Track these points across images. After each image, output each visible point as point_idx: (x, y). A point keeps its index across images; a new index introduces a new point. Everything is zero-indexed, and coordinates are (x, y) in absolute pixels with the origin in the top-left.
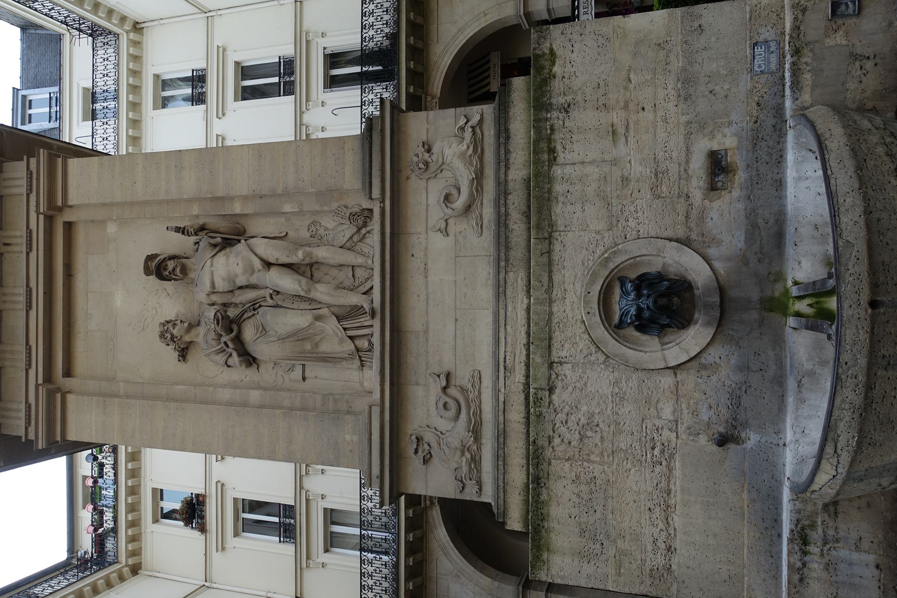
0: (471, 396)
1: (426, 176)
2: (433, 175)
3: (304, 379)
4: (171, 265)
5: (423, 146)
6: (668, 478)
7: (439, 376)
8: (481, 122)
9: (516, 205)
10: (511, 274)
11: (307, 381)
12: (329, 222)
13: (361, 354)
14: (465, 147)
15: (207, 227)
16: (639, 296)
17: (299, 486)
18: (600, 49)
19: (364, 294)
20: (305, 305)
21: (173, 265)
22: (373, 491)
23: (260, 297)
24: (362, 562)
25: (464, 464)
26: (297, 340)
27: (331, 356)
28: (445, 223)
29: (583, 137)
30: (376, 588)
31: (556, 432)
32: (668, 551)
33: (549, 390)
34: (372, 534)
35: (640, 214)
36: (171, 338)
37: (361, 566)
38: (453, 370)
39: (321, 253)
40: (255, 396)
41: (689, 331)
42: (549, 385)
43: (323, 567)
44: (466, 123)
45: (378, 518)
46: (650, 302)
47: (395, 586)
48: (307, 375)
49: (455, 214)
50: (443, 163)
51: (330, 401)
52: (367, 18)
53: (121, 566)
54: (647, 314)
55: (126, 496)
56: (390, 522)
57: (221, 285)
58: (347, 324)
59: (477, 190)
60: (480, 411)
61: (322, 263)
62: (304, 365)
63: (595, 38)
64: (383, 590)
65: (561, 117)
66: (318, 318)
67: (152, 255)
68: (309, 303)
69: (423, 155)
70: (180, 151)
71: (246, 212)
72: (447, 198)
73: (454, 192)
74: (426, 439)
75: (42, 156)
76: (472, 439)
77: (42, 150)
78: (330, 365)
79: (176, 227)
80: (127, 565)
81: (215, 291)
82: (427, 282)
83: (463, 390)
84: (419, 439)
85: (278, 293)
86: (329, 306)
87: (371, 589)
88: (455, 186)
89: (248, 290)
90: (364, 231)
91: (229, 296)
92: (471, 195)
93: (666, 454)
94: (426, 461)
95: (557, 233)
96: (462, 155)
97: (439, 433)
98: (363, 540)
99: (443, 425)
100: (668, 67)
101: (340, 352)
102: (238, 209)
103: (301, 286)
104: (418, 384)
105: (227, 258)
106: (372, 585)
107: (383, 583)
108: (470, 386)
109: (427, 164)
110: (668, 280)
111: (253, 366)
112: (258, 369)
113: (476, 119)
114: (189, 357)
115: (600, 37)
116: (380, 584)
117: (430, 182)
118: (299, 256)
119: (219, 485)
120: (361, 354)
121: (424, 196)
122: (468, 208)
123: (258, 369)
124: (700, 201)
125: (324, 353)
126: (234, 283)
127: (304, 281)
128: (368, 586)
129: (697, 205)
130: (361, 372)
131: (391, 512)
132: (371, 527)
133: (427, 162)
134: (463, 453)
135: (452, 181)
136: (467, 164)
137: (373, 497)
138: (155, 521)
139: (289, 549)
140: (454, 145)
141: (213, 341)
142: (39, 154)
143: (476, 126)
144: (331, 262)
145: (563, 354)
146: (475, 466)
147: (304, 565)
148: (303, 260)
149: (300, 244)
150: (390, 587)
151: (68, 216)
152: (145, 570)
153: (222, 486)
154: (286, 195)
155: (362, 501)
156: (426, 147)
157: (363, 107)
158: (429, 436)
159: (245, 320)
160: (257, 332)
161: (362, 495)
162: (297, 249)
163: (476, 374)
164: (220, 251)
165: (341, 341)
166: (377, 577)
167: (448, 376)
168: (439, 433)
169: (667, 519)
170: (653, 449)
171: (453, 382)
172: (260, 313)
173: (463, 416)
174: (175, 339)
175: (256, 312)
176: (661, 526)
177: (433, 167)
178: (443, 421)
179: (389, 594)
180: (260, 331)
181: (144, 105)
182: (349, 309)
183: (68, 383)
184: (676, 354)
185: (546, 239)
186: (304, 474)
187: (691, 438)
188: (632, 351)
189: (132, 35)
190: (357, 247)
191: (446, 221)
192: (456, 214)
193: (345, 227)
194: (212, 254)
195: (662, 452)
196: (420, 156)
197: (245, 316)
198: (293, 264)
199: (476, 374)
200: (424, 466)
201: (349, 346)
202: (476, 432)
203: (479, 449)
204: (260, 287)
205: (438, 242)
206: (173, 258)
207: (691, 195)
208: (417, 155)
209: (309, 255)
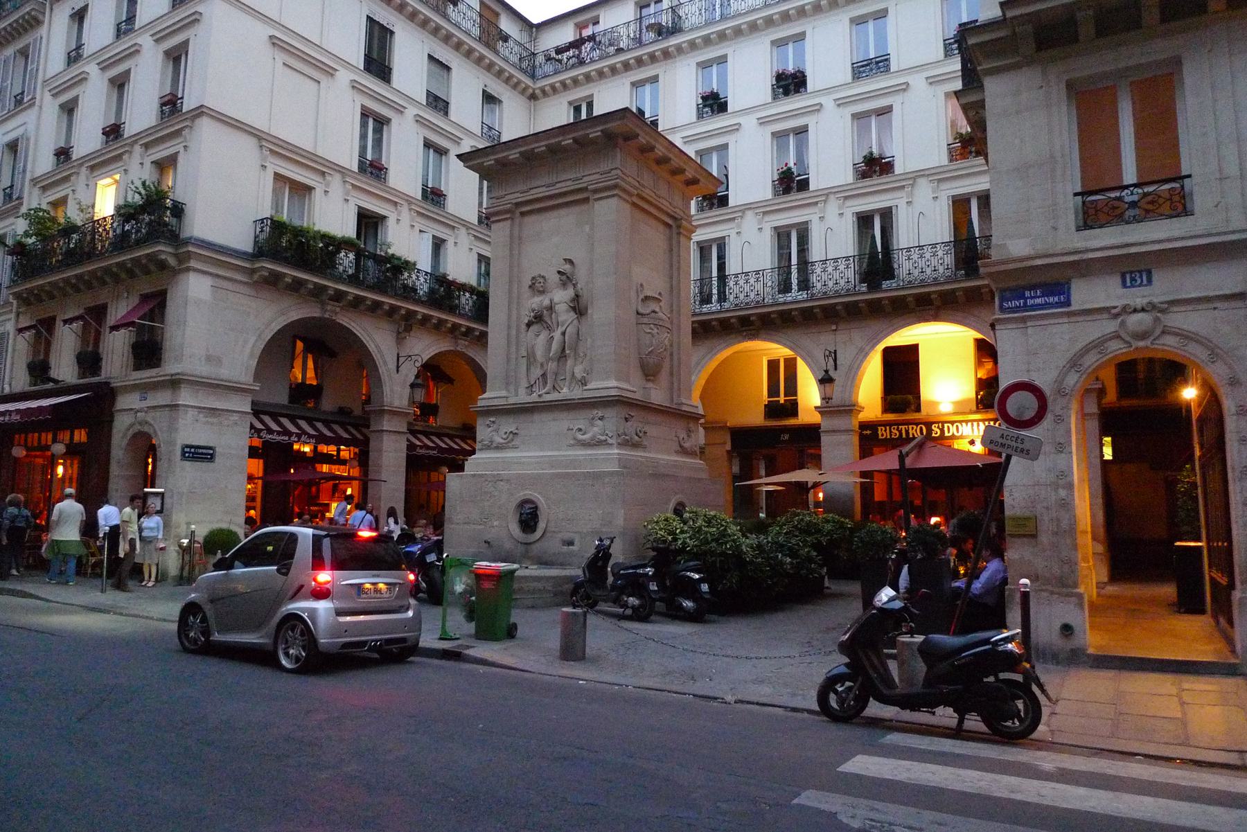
10: (582, 421)
17: (827, 193)
24: (934, 245)
53: (532, 85)
55: (621, 62)
80: (534, 90)
87: (921, 257)
113: (610, 441)
119: (904, 87)
128: (936, 252)
138: (570, 103)
139: (768, 193)
152: (534, 106)
153: (736, 128)
166: (747, 288)
181: (697, 53)
187: (1172, 627)
189: (531, 91)
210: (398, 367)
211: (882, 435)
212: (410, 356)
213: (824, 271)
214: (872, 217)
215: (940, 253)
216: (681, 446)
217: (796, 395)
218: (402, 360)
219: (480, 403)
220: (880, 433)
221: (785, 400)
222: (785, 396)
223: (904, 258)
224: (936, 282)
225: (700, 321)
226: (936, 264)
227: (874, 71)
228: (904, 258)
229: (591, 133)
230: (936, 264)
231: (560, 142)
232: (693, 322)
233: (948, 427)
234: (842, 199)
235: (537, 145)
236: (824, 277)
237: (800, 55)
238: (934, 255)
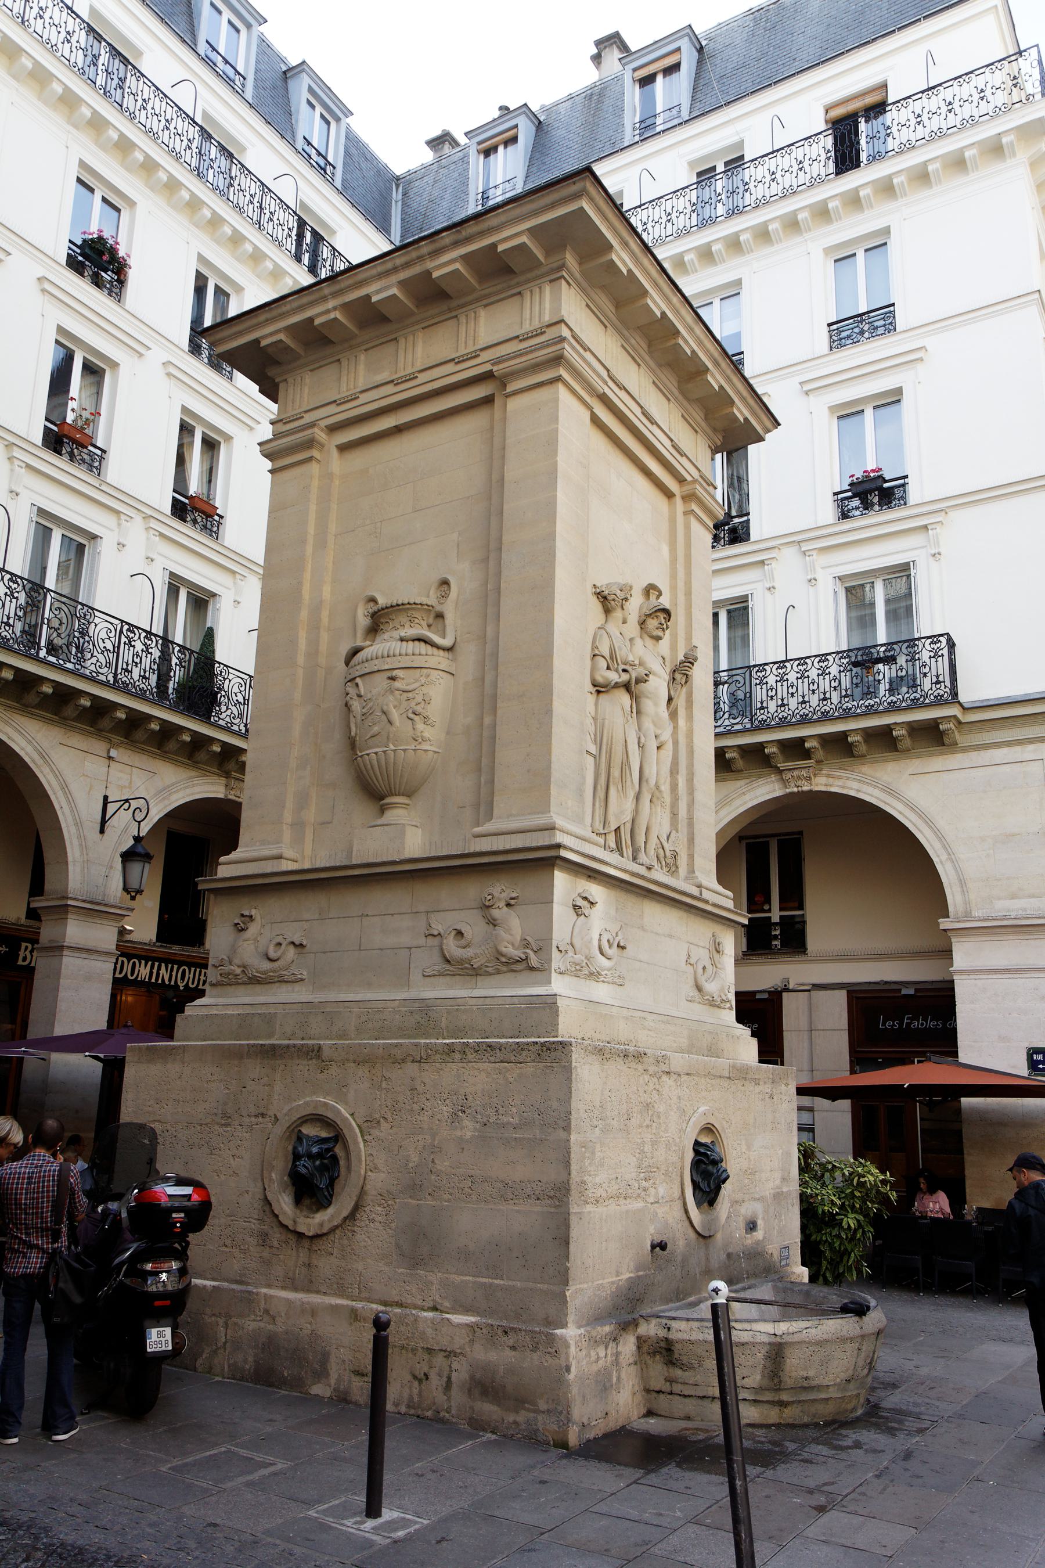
24: (823, 657)
30: (785, 688)
34: (942, 655)
37: (904, 642)
41: (291, 1206)
45: (859, 681)
47: (927, 701)
52: (142, 639)
56: (811, 709)
64: (782, 700)
98: (818, 659)
106: (767, 683)
107: (795, 698)
116: (792, 694)
131: (828, 709)
132: (756, 684)
137: (827, 677)
147: (805, 547)
150: (811, 709)
153: (913, 359)
155: (906, 644)
161: (807, 661)
179: (934, 689)
186: (803, 549)
210: (104, 822)
211: (24, 959)
212: (127, 801)
213: (782, 679)
215: (834, 670)
216: (699, 989)
217: (801, 907)
218: (111, 809)
219: (223, 872)
220: (22, 954)
221: (781, 917)
222: (781, 909)
226: (827, 689)
227: (866, 335)
228: (754, 681)
233: (123, 962)
236: (782, 690)
237: (879, 277)
238: (823, 673)
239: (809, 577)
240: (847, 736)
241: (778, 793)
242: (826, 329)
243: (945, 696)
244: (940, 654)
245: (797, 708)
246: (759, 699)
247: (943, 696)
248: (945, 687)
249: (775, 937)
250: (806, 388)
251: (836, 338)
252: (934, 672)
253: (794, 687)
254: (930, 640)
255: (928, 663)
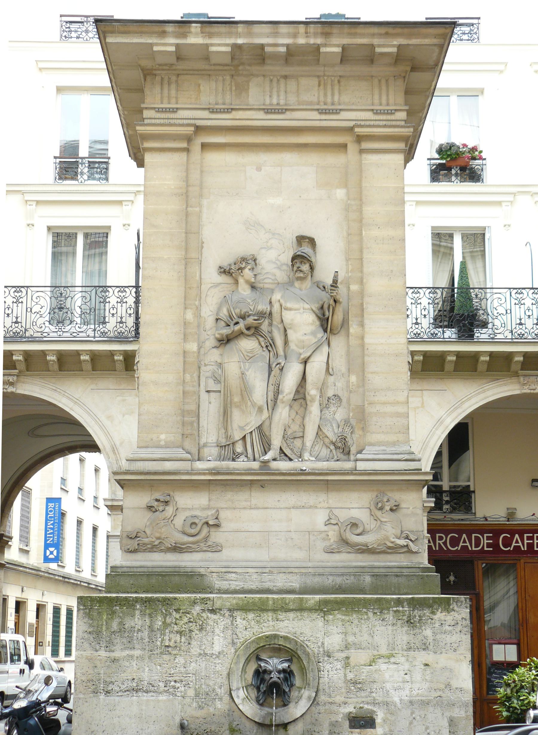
0: (202, 545)
1: (373, 508)
2: (373, 514)
3: (208, 392)
4: (305, 267)
5: (395, 506)
6: (156, 692)
7: (217, 518)
8: (410, 552)
9: (346, 581)
11: (207, 394)
12: (340, 414)
13: (231, 446)
14: (393, 540)
15: (337, 304)
16: (279, 672)
18: (449, 645)
19: (281, 449)
20: (271, 395)
21: (305, 269)
22: (11, 305)
23: (278, 350)
25: (150, 539)
26: (241, 390)
27: (229, 420)
28: (335, 523)
29: (389, 633)
31: (183, 615)
32: (107, 692)
33: (213, 609)
34: (22, 302)
35: (335, 672)
36: (241, 268)
38: (221, 530)
39: (314, 409)
40: (193, 347)
42: (216, 609)
43: (28, 225)
44: (411, 540)
46: (275, 679)
48: (211, 394)
49: (342, 531)
50: (381, 521)
51: (191, 419)
54: (267, 677)
57: (288, 316)
58: (255, 436)
59: (359, 549)
60: (191, 552)
61: (306, 409)
62: (220, 392)
63: (457, 642)
65: (404, 618)
66: (260, 409)
67: (315, 245)
68: (273, 399)
69: (388, 506)
70: (405, 275)
71: (350, 337)
72: (354, 525)
73: (359, 531)
74: (167, 508)
75: (407, 130)
76: (170, 546)
77: (412, 130)
78: (221, 419)
79: (337, 281)
81: (283, 309)
82: (290, 508)
83: (206, 539)
84: (167, 503)
85: (282, 370)
86: (270, 418)
88: (363, 531)
89: (283, 338)
90: (332, 447)
91: (279, 320)
92: (357, 545)
93: (172, 690)
94: (150, 508)
95: (323, 615)
96: (387, 538)
97: (172, 518)
99: (179, 522)
100: (433, 690)
101: (232, 429)
102: (354, 329)
103: (286, 395)
104: (209, 500)
105: (311, 324)
108: (209, 543)
109: (381, 509)
110: (290, 691)
111: (218, 342)
112: (215, 347)
114: (223, 275)
115: (457, 645)
117: (368, 510)
118: (312, 391)
119: (501, 67)
120: (231, 446)
121: (356, 505)
122: (345, 542)
123: (215, 347)
124: (342, 711)
125: (231, 412)
126: (290, 328)
127: (291, 396)
129: (340, 710)
130: (215, 444)
132: (100, 302)
133: (382, 509)
134: (158, 538)
135: (367, 527)
136: (379, 541)
137: (124, 305)
140: (394, 531)
141: (239, 310)
142: (408, 127)
143: (408, 548)
144: (307, 419)
145: (238, 619)
146: (149, 548)
147: (28, 197)
148: (308, 394)
149: (322, 390)
150: (127, 329)
151: (352, 148)
154: (363, 380)
156: (394, 508)
157: (532, 291)
158: (170, 510)
159: (258, 339)
160: (248, 352)
162: (318, 389)
163: (219, 548)
164: (317, 316)
165: (242, 428)
167: (217, 526)
168: (172, 518)
169: (128, 691)
170: (175, 681)
171: (213, 529)
172: (263, 353)
173: (186, 539)
174: (240, 271)
175: (265, 349)
176: (123, 687)
177: (379, 513)
178: (182, 522)
179: (13, 327)
180: (248, 354)
182: (267, 434)
183: (196, 147)
184: (240, 695)
185: (319, 607)
186: (26, 198)
188: (241, 667)
190: (319, 440)
191: (337, 524)
192: (342, 533)
193: (336, 431)
194: (314, 309)
195: (174, 687)
196: (388, 504)
197: (261, 339)
198: (305, 381)
199: (219, 548)
200: (146, 506)
201: (237, 436)
202: (176, 549)
203: (162, 551)
204: (287, 348)
205: (321, 517)
206: (312, 268)
207: (346, 705)
208: (388, 501)
209: (313, 400)
214: (451, 236)
222: (450, 481)
223: (24, 300)
224: (521, 339)
225: (459, 352)
226: (124, 314)
228: (513, 301)
229: (157, 44)
230: (124, 314)
231: (151, 45)
232: (413, 353)
234: (414, 203)
235: (270, 41)
239: (28, 223)
240: (12, 355)
241: (517, 392)
242: (59, 19)
243: (21, 334)
244: (20, 301)
245: (11, 326)
246: (518, 317)
247: (124, 333)
248: (22, 327)
249: (447, 502)
250: (41, 65)
251: (474, 36)
252: (15, 314)
253: (10, 309)
254: (14, 289)
255: (11, 307)
